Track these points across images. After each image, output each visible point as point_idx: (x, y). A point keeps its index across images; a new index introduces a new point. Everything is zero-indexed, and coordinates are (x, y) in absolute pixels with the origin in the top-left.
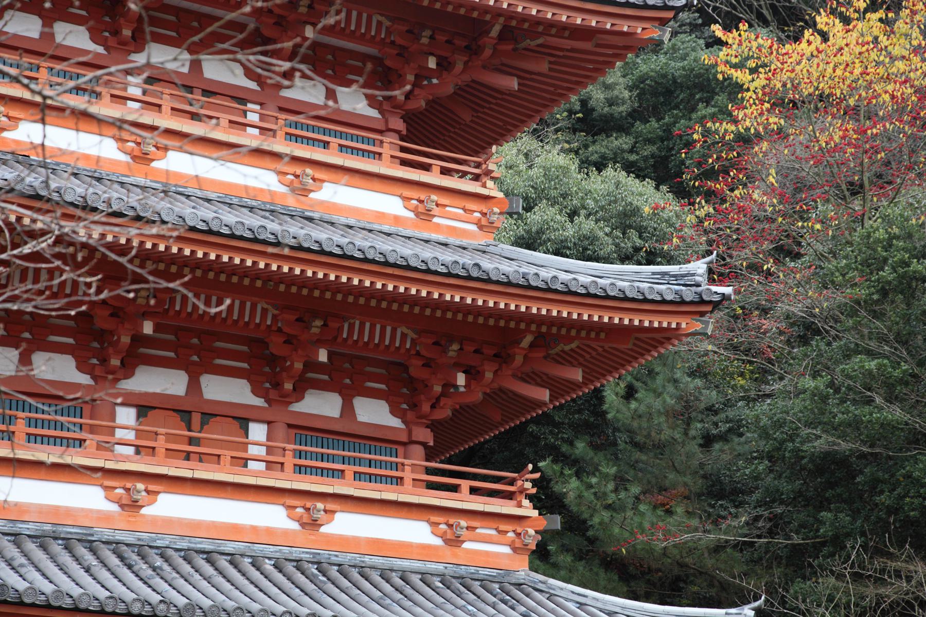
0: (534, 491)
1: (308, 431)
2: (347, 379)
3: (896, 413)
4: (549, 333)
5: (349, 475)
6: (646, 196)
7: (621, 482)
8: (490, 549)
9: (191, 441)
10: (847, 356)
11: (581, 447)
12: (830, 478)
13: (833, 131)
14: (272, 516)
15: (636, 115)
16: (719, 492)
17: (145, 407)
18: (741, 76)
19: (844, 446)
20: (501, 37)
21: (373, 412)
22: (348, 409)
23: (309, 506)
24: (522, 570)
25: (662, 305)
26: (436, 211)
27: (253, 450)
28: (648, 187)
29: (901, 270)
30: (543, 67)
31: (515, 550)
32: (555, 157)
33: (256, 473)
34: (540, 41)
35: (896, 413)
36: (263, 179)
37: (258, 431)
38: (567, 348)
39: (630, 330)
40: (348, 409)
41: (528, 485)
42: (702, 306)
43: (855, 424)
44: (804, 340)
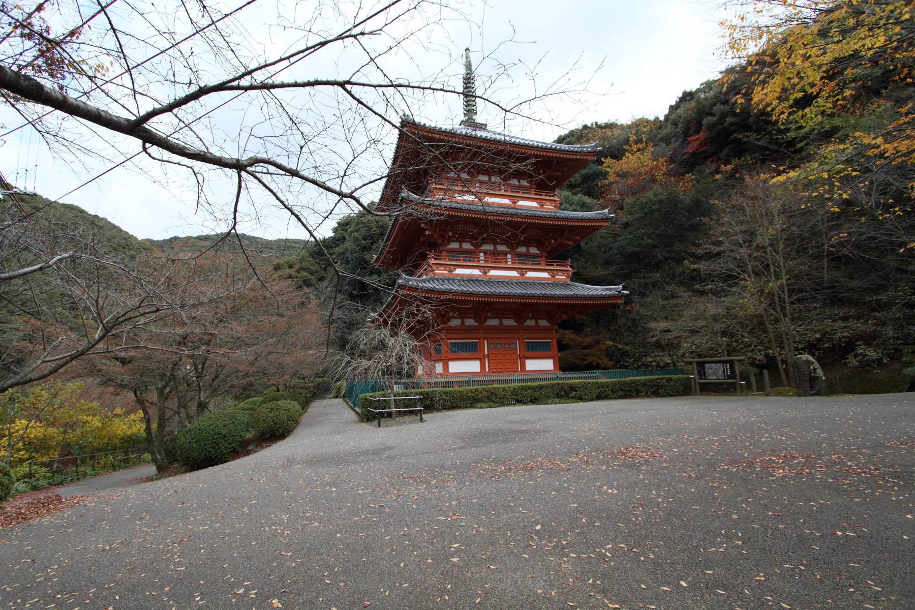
2: (527, 243)
3: (650, 241)
4: (572, 229)
6: (588, 200)
7: (586, 263)
8: (561, 277)
10: (113, 466)
11: (576, 256)
12: (633, 257)
13: (630, 181)
14: (514, 274)
15: (582, 183)
16: (607, 263)
17: (485, 253)
18: (608, 170)
19: (637, 250)
21: (534, 250)
22: (528, 250)
23: (522, 271)
24: (569, 281)
25: (598, 220)
28: (587, 198)
30: (566, 169)
32: (566, 193)
33: (509, 264)
35: (650, 241)
36: (506, 201)
37: (509, 256)
39: (589, 227)
40: (528, 250)
42: (607, 219)
43: (639, 245)
44: (625, 228)
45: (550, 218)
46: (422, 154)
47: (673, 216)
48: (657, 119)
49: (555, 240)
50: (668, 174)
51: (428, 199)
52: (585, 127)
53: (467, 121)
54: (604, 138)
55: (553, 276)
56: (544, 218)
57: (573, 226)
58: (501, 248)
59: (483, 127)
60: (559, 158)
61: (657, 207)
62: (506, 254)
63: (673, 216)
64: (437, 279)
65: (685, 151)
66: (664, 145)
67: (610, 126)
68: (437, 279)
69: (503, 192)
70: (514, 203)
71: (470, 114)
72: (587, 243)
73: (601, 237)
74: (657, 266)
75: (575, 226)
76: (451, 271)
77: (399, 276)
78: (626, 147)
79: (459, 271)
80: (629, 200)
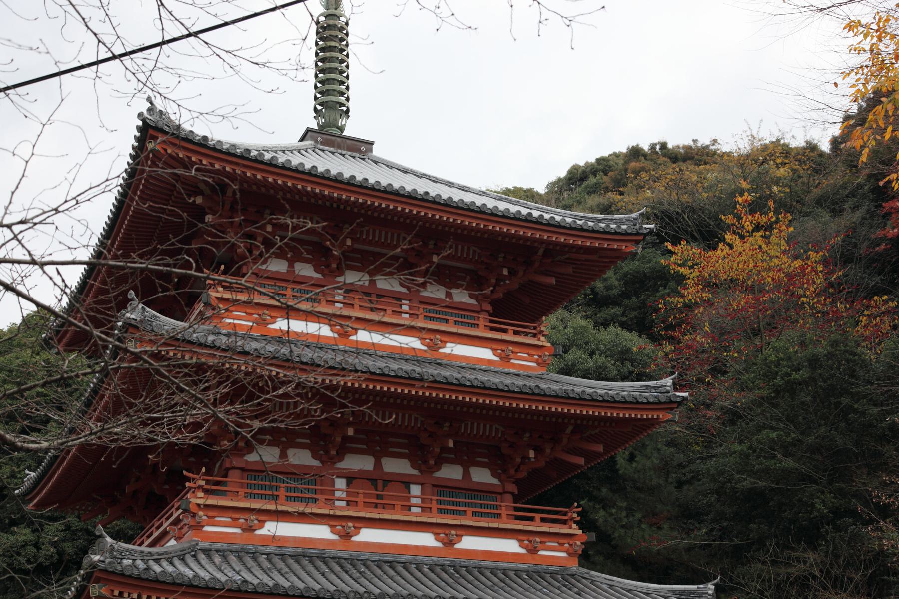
0: (579, 518)
1: (444, 488)
2: (466, 456)
3: (790, 463)
4: (582, 425)
5: (470, 513)
6: (635, 342)
7: (630, 511)
8: (554, 554)
9: (378, 497)
13: (740, 300)
14: (426, 539)
15: (625, 295)
16: (688, 515)
17: (350, 479)
18: (684, 270)
20: (545, 255)
21: (482, 476)
22: (467, 475)
23: (448, 533)
24: (574, 566)
26: (512, 356)
27: (414, 501)
29: (786, 379)
30: (570, 270)
31: (569, 554)
34: (567, 256)
35: (790, 463)
37: (415, 490)
38: (593, 433)
40: (467, 475)
41: (575, 515)
42: (672, 404)
44: (732, 423)
45: (522, 394)
46: (188, 207)
47: (845, 401)
48: (812, 147)
49: (538, 450)
50: (832, 290)
51: (199, 332)
52: (635, 153)
53: (321, 130)
54: (677, 185)
55: (533, 551)
56: (507, 393)
57: (581, 417)
58: (396, 466)
59: (360, 148)
60: (549, 242)
61: (804, 374)
62: (406, 483)
63: (845, 401)
64: (207, 552)
65: (879, 233)
66: (827, 217)
67: (698, 156)
68: (207, 552)
69: (405, 319)
70: (433, 348)
71: (332, 114)
72: (632, 458)
73: (669, 444)
74: (811, 535)
75: (588, 418)
76: (250, 529)
77: (92, 539)
78: (728, 219)
79: (271, 528)
80: (737, 352)
